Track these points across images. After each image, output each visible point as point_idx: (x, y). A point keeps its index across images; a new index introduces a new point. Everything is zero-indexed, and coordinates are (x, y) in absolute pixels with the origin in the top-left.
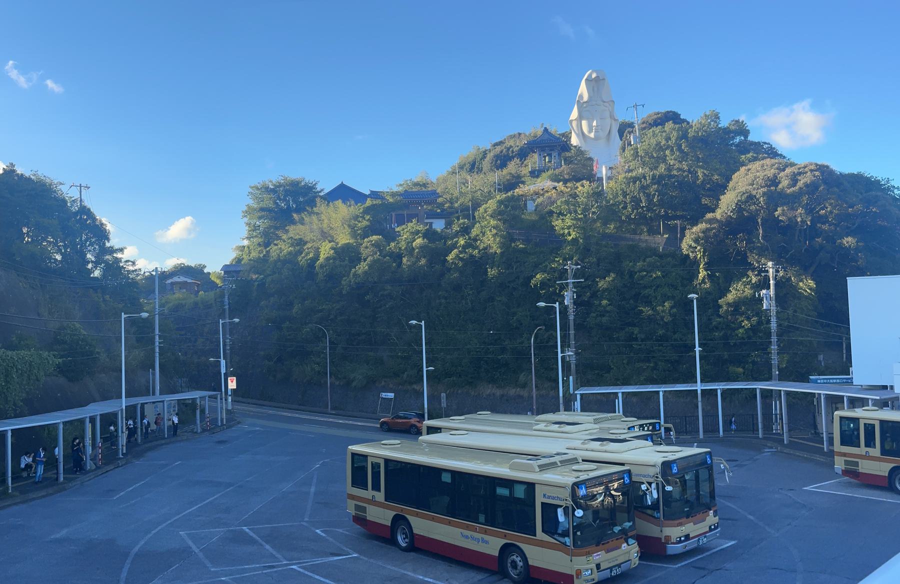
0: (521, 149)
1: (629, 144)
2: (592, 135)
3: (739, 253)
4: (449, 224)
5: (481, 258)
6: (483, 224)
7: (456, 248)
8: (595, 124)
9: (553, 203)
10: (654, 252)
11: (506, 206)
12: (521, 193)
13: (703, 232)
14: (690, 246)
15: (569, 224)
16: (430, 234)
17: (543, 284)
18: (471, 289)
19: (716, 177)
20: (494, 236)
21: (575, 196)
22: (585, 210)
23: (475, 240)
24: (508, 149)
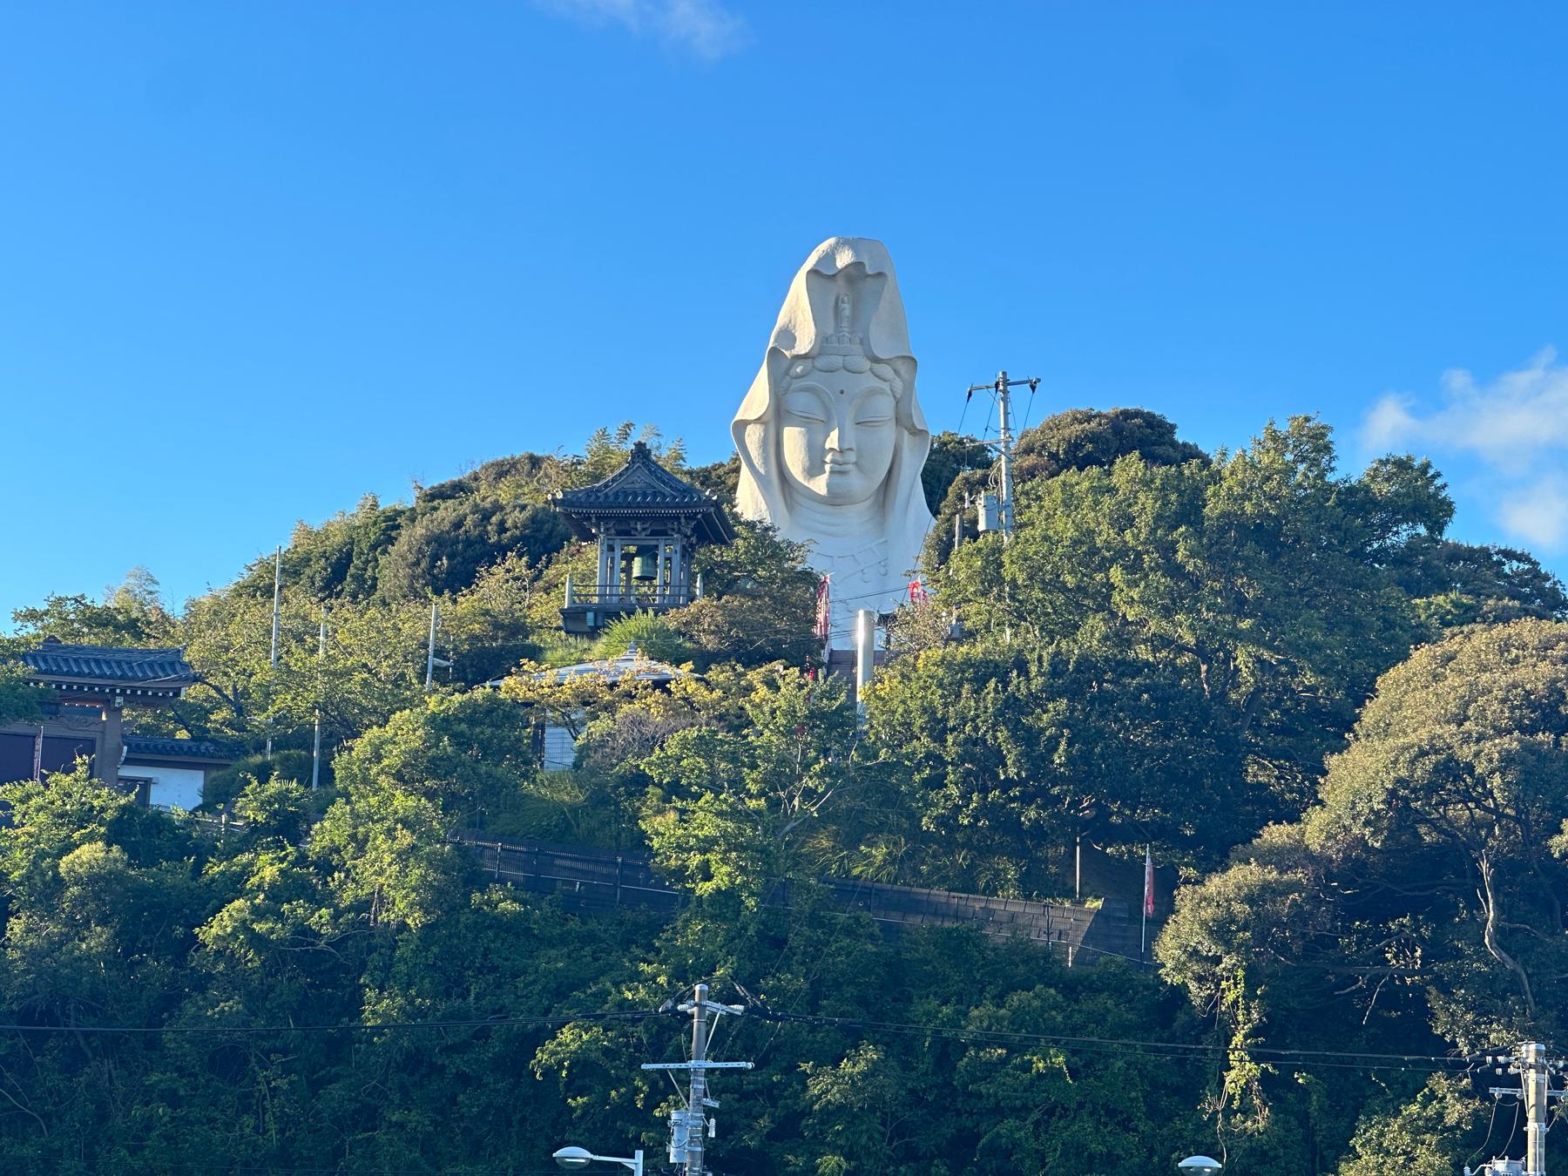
0: (536, 521)
1: (971, 532)
2: (820, 485)
3: (1392, 997)
4: (219, 796)
5: (338, 944)
6: (361, 806)
7: (239, 894)
8: (833, 441)
9: (649, 743)
10: (1037, 965)
11: (461, 742)
12: (523, 694)
13: (1250, 900)
14: (1195, 954)
15: (709, 831)
16: (138, 830)
17: (584, 1069)
18: (287, 1070)
19: (1309, 679)
20: (403, 856)
21: (738, 722)
22: (779, 780)
23: (326, 867)
24: (486, 516)
